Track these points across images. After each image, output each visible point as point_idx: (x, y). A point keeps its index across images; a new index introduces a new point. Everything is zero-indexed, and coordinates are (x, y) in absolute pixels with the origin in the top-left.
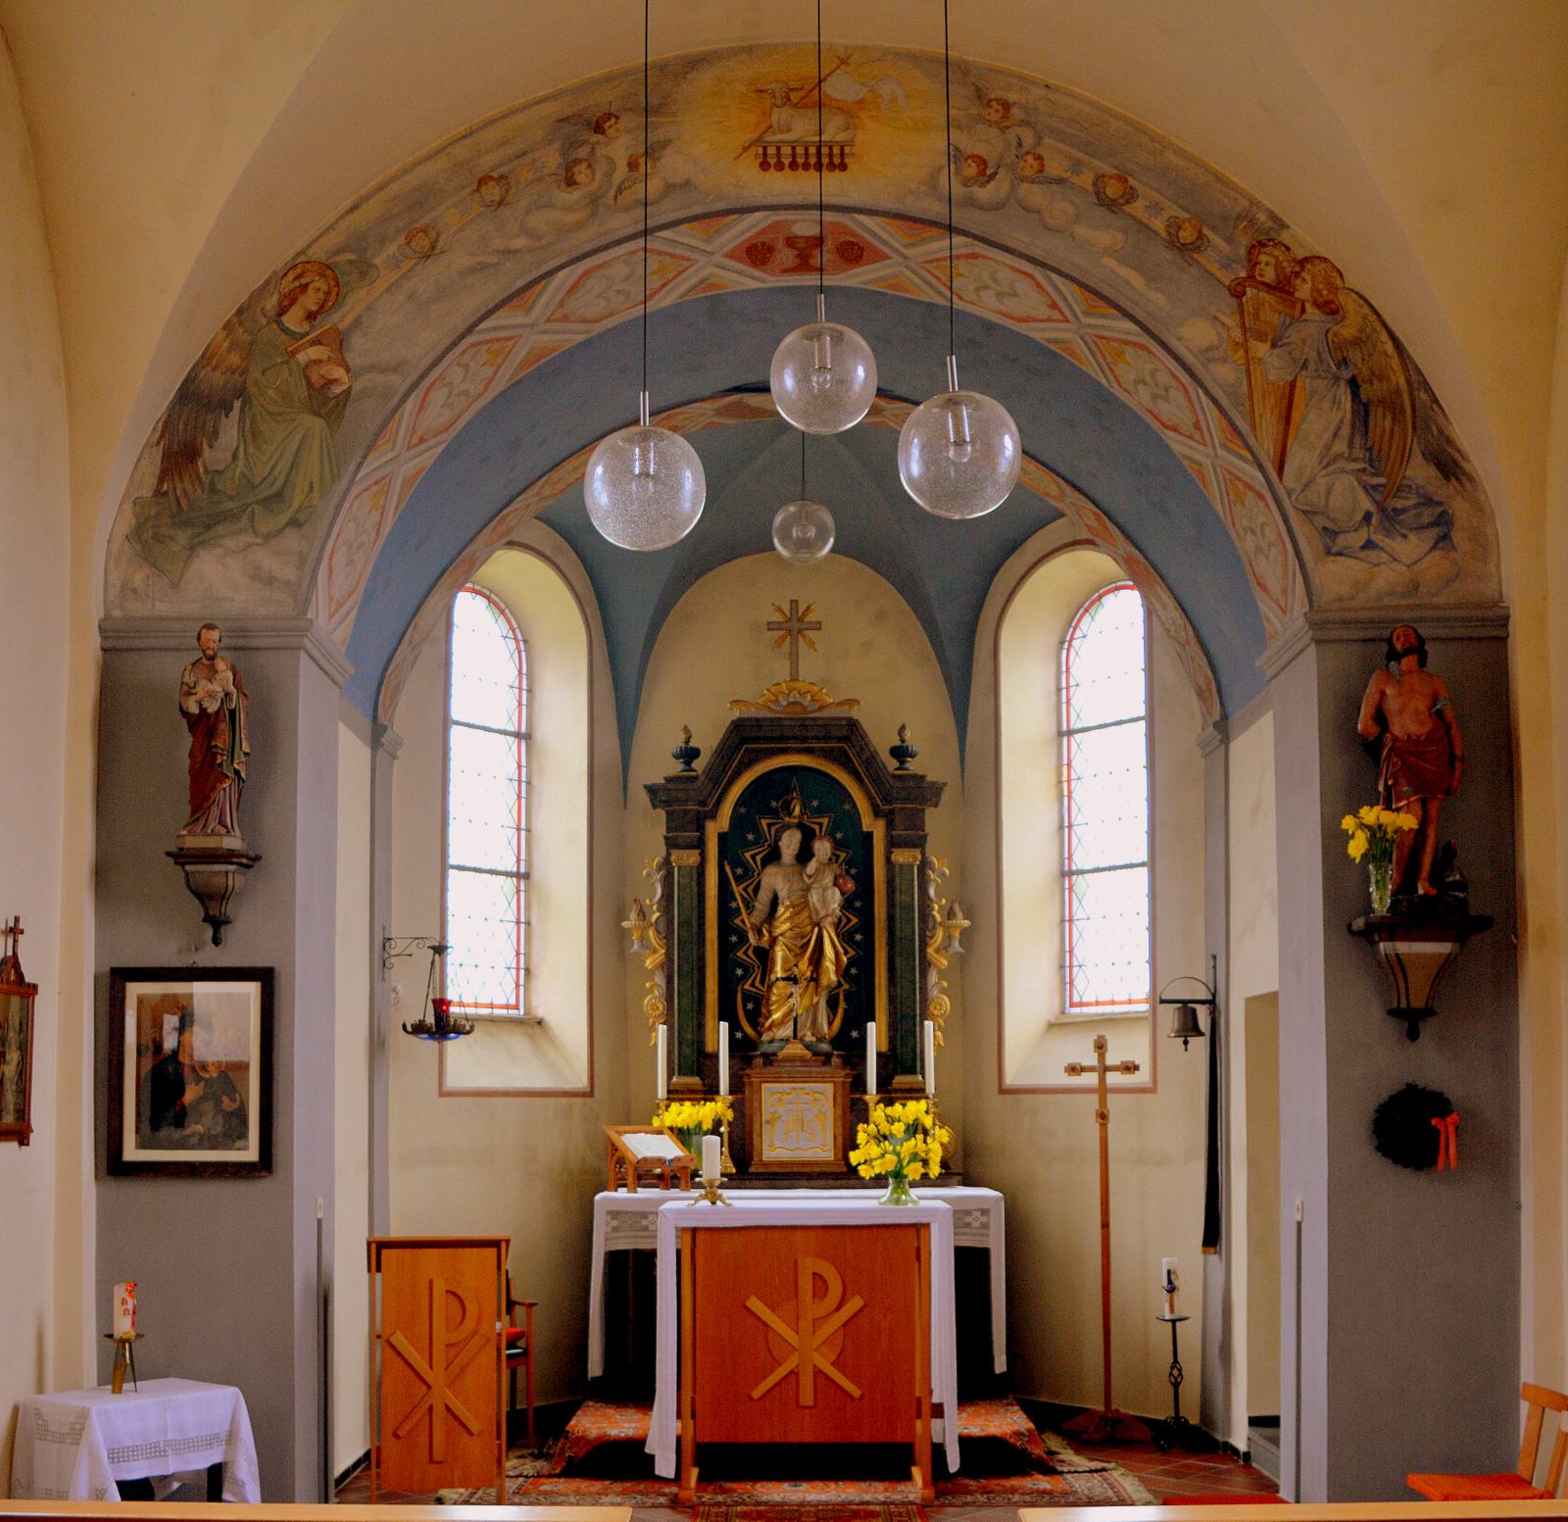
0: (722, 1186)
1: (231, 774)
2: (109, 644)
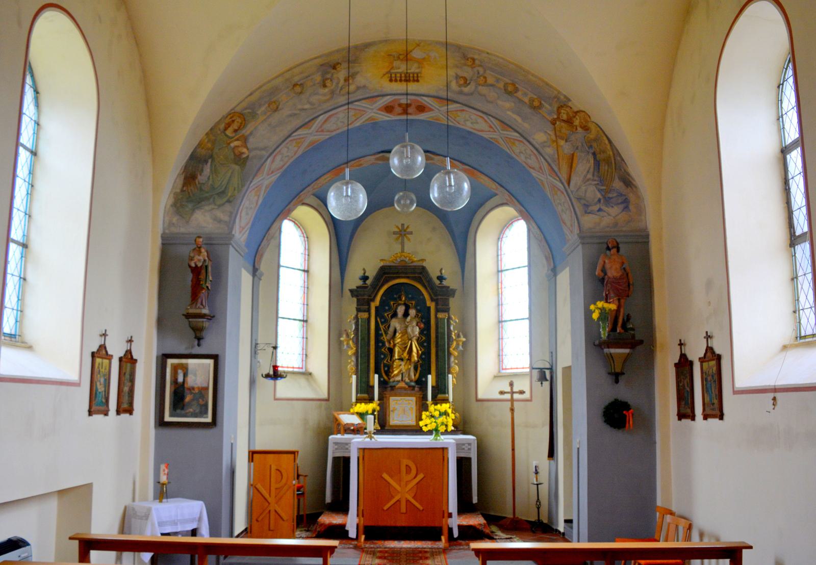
0: (374, 433)
1: (205, 288)
2: (165, 242)
